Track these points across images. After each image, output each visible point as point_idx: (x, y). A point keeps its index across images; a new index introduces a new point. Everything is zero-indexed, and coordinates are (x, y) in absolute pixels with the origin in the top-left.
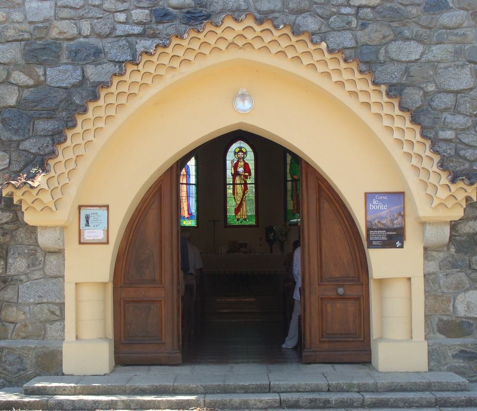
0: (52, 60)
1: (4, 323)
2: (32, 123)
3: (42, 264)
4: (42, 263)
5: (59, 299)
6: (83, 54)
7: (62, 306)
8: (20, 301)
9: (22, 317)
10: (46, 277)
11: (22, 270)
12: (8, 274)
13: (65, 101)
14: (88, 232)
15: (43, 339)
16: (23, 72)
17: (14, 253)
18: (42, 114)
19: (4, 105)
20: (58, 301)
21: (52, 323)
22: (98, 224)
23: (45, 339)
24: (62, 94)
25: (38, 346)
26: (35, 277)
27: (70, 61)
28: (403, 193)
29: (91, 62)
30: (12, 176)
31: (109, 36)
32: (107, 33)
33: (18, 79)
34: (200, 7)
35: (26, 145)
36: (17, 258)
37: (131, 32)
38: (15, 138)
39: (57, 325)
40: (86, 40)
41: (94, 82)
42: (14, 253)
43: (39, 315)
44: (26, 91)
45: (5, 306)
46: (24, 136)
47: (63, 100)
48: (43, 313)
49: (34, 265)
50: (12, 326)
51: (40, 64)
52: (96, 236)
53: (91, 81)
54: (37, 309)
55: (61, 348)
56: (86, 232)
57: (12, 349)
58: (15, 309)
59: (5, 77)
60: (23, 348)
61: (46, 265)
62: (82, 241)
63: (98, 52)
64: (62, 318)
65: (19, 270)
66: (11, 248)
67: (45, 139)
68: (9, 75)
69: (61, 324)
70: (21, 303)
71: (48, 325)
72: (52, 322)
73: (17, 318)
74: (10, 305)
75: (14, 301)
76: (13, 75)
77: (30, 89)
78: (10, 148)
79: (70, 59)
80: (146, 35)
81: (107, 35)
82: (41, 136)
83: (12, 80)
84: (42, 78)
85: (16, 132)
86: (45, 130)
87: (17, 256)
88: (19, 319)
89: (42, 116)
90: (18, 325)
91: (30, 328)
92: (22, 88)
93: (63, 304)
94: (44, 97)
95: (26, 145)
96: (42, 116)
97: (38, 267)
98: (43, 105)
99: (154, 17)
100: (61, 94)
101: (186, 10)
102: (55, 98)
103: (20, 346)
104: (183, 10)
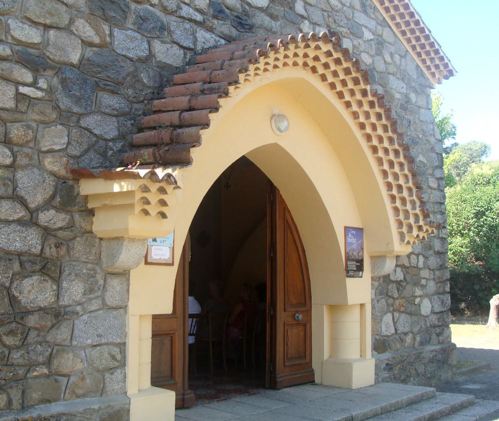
0: (119, 20)
1: (57, 377)
2: (96, 94)
3: (101, 289)
4: (101, 288)
5: (120, 338)
6: (150, 25)
7: (122, 346)
8: (75, 343)
9: (80, 366)
10: (105, 307)
11: (78, 299)
12: (60, 303)
13: (131, 75)
14: (156, 249)
15: (101, 396)
16: (90, 24)
17: (70, 274)
18: (108, 85)
19: (66, 60)
20: (118, 341)
21: (111, 371)
22: (164, 240)
23: (104, 395)
24: (129, 67)
25: (102, 407)
26: (93, 308)
27: (135, 28)
28: (362, 229)
29: (155, 36)
30: (70, 161)
31: (173, 14)
32: (173, 10)
33: (82, 30)
34: (245, 15)
35: (90, 121)
36: (73, 280)
37: (194, 17)
38: (76, 109)
39: (118, 374)
40: (151, 8)
41: (160, 62)
42: (70, 274)
43: (97, 362)
44: (89, 49)
45: (58, 351)
46: (86, 109)
47: (130, 74)
48: (101, 357)
49: (91, 291)
50: (65, 380)
51: (106, 20)
52: (162, 255)
53: (158, 59)
54: (95, 353)
55: (127, 406)
56: (153, 248)
57: (71, 415)
58: (71, 355)
59: (67, 22)
60: (85, 411)
61: (106, 291)
62: (149, 260)
63: (163, 28)
64: (123, 364)
65: (73, 297)
66: (65, 267)
67: (110, 118)
68: (72, 22)
69: (121, 372)
70: (76, 346)
71: (107, 375)
72: (111, 370)
73: (73, 367)
74: (64, 350)
75: (67, 344)
76: (77, 23)
77: (94, 49)
78: (69, 122)
79: (136, 26)
80: (205, 26)
81: (173, 12)
82: (105, 113)
83: (74, 30)
84: (108, 39)
85: (78, 100)
86: (110, 106)
87: (73, 278)
88: (75, 369)
89: (107, 88)
90: (72, 379)
91: (88, 381)
92: (87, 44)
93: (124, 344)
94: (110, 63)
95: (90, 121)
96: (107, 88)
97: (96, 294)
98: (109, 74)
99: (212, 10)
100: (129, 66)
101: (236, 14)
102: (122, 69)
103: (81, 409)
104: (233, 13)
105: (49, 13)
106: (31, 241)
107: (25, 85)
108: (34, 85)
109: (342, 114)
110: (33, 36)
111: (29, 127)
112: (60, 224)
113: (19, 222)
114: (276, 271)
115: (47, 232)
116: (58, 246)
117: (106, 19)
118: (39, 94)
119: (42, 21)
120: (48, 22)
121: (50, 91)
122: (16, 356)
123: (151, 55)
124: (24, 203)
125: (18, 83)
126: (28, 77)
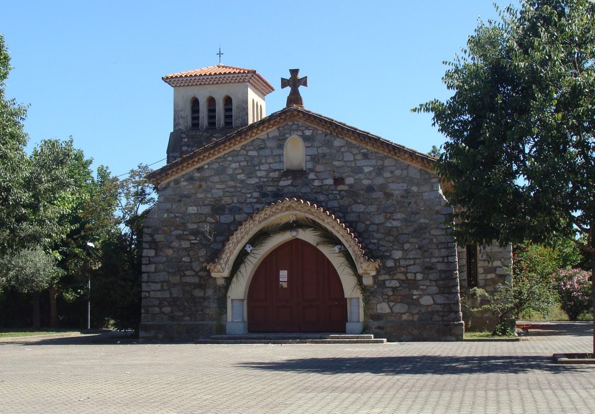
92: (211, 223)
105: (199, 219)
106: (196, 280)
107: (192, 240)
108: (196, 239)
109: (339, 272)
110: (195, 226)
111: (195, 251)
112: (204, 275)
113: (193, 275)
114: (281, 343)
115: (201, 277)
116: (204, 280)
117: (218, 214)
118: (197, 242)
119: (196, 221)
120: (198, 221)
121: (201, 239)
122: (193, 309)
123: (235, 219)
124: (194, 271)
125: (190, 240)
126: (194, 238)
